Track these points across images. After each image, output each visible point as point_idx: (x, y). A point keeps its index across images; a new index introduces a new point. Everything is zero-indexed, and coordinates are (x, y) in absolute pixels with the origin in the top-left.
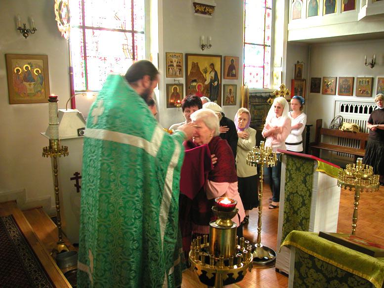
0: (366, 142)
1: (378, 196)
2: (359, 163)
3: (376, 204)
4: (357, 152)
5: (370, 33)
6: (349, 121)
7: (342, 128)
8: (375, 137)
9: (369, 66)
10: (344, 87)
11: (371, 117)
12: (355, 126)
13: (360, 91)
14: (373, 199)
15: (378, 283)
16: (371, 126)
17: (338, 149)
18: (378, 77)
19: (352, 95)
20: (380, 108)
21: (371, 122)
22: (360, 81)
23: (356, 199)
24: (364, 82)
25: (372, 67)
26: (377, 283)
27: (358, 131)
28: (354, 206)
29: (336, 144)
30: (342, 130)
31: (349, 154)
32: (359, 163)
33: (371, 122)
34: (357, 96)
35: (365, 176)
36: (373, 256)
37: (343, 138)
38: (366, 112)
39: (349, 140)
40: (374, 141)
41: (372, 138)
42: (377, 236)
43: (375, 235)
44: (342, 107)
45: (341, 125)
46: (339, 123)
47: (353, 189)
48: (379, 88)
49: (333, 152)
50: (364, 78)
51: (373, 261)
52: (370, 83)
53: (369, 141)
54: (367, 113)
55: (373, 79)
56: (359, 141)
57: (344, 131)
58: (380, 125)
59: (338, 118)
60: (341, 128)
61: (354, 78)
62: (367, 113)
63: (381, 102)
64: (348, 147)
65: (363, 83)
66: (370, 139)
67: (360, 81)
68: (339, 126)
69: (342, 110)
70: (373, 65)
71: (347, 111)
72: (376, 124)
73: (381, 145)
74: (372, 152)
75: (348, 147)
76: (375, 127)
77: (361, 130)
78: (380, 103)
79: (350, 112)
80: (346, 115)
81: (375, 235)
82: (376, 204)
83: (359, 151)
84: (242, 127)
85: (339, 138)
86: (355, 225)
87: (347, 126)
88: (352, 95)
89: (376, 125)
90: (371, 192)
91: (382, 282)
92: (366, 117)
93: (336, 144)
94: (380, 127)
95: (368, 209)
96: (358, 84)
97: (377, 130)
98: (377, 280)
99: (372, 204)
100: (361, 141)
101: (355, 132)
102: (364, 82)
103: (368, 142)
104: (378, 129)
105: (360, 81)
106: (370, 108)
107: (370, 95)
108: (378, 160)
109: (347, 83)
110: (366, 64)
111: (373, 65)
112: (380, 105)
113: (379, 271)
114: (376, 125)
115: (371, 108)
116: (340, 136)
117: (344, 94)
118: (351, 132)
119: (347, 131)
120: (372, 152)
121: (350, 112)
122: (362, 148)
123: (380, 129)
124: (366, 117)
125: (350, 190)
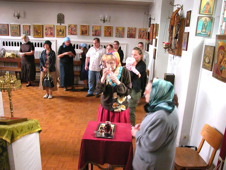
0: (21, 63)
1: (31, 93)
2: (7, 75)
3: (30, 97)
4: (17, 70)
5: (148, 2)
6: (9, 51)
7: (6, 56)
8: (25, 59)
9: (17, 18)
10: (3, 30)
11: (21, 48)
12: (13, 54)
13: (13, 33)
14: (29, 95)
15: (8, 138)
16: (21, 54)
17: (5, 69)
18: (22, 24)
19: (9, 35)
20: (25, 43)
21: (21, 51)
22: (13, 26)
23: (10, 96)
24: (15, 27)
25: (104, 23)
26: (7, 138)
27: (15, 57)
28: (9, 100)
29: (4, 66)
30: (5, 57)
31: (12, 71)
32: (7, 75)
33: (21, 51)
34: (12, 36)
35: (12, 81)
36: (6, 125)
37: (9, 62)
38: (18, 46)
39: (15, 63)
40: (24, 62)
41: (23, 61)
42: (32, 114)
43: (30, 114)
44: (4, 43)
45: (4, 54)
46: (3, 53)
47: (6, 90)
48: (24, 31)
49: (2, 71)
50: (14, 25)
51: (4, 128)
52: (18, 28)
53: (22, 62)
54: (39, 47)
55: (20, 26)
56: (17, 63)
57: (7, 58)
58: (26, 53)
59: (2, 50)
60: (5, 56)
61: (8, 25)
62: (42, 47)
63: (25, 39)
64: (7, 67)
65: (14, 28)
66: (22, 61)
67: (12, 27)
68: (3, 55)
69: (4, 45)
70: (18, 17)
71: (7, 45)
72: (24, 52)
73: (28, 64)
74: (24, 69)
75: (7, 67)
76: (24, 54)
77: (17, 56)
78: (24, 40)
79: (15, 46)
80: (7, 48)
81: (30, 114)
82: (30, 97)
83: (17, 69)
84: (113, 70)
85: (4, 62)
86: (12, 111)
87: (8, 54)
88: (9, 35)
89: (24, 53)
90: (17, 90)
91: (10, 137)
92: (18, 48)
93: (4, 66)
94: (27, 54)
95: (26, 101)
96: (11, 28)
97: (25, 56)
98: (7, 137)
99: (28, 98)
100: (18, 63)
101: (13, 58)
102: (15, 27)
103: (21, 63)
104: (26, 55)
105: (12, 27)
106: (6, 42)
107: (19, 35)
108: (28, 73)
109: (4, 28)
110: (14, 16)
111: (18, 17)
112: (25, 41)
113: (7, 132)
114: (24, 53)
115: (21, 43)
116: (5, 61)
117: (4, 34)
118: (11, 58)
119: (9, 58)
120: (24, 69)
121: (15, 46)
122: (19, 67)
123: (27, 55)
124: (18, 48)
125: (4, 91)
